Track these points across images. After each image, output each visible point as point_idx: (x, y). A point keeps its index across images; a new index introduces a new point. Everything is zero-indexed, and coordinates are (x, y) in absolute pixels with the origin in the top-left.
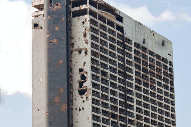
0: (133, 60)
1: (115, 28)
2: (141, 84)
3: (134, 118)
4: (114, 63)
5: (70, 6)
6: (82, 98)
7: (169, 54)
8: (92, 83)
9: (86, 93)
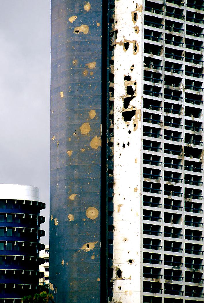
6: (128, 125)
8: (145, 100)
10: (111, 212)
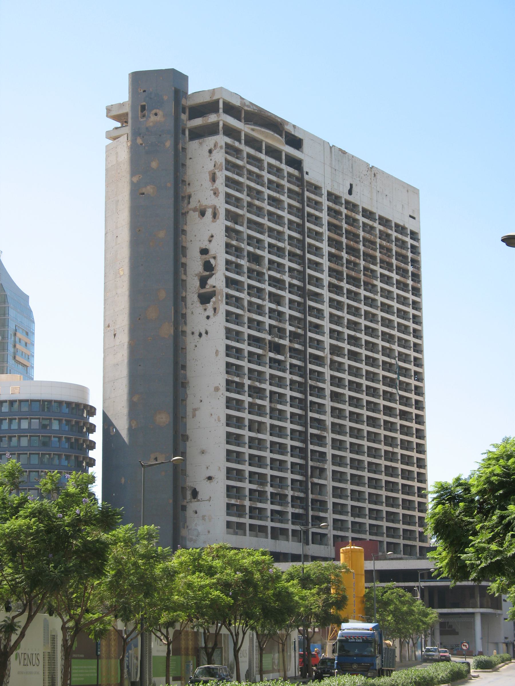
0: (324, 230)
1: (284, 161)
2: (341, 280)
3: (324, 352)
4: (279, 235)
5: (184, 117)
6: (205, 310)
7: (411, 216)
8: (227, 279)
9: (214, 299)
10: (184, 417)
